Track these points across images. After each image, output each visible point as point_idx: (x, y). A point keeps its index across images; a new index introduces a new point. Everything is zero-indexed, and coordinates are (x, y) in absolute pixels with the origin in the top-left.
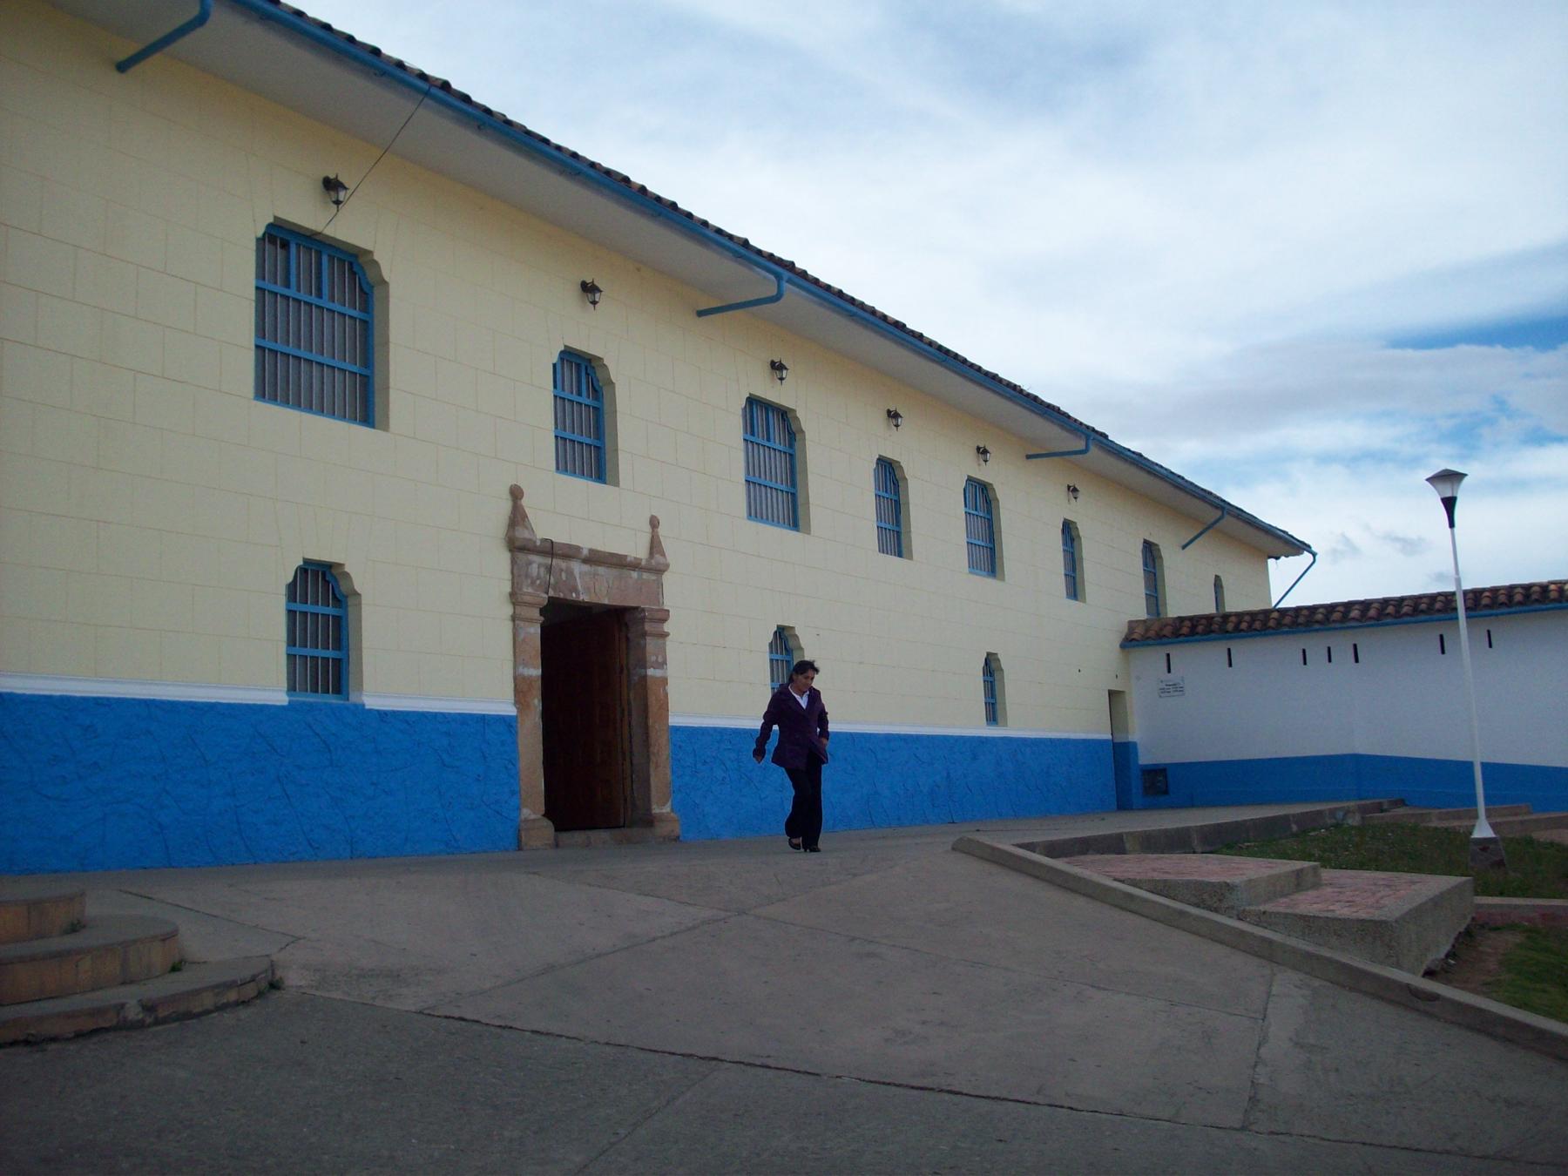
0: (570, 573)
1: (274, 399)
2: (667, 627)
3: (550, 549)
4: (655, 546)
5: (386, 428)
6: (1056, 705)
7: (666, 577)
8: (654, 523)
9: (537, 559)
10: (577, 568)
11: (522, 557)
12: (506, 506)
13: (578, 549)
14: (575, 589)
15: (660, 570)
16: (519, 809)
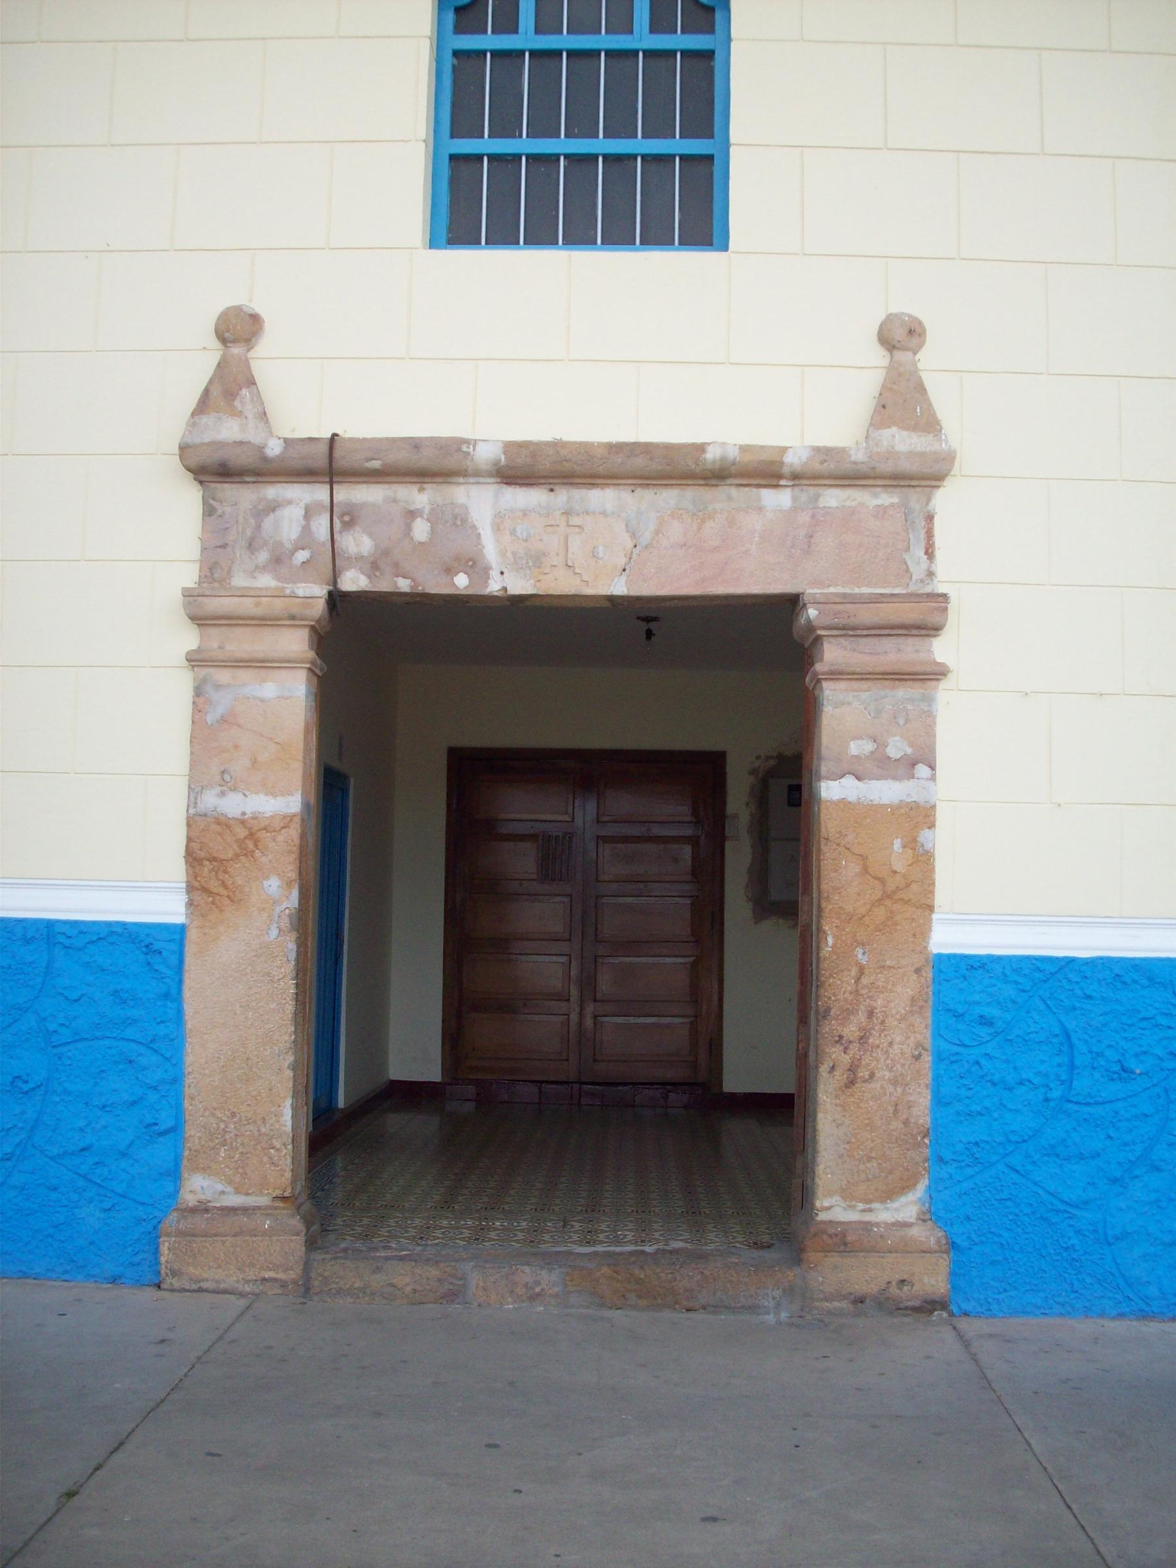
0: (460, 521)
1: (503, 235)
2: (941, 649)
3: (329, 464)
4: (902, 400)
5: (725, 248)
6: (269, 1203)
7: (946, 502)
8: (900, 337)
9: (301, 496)
10: (482, 503)
11: (241, 498)
12: (203, 362)
13: (456, 446)
14: (474, 564)
15: (924, 477)
16: (174, 1174)
